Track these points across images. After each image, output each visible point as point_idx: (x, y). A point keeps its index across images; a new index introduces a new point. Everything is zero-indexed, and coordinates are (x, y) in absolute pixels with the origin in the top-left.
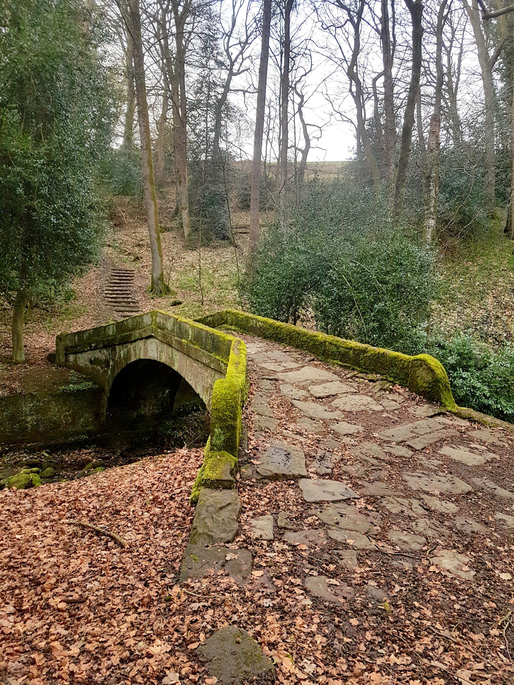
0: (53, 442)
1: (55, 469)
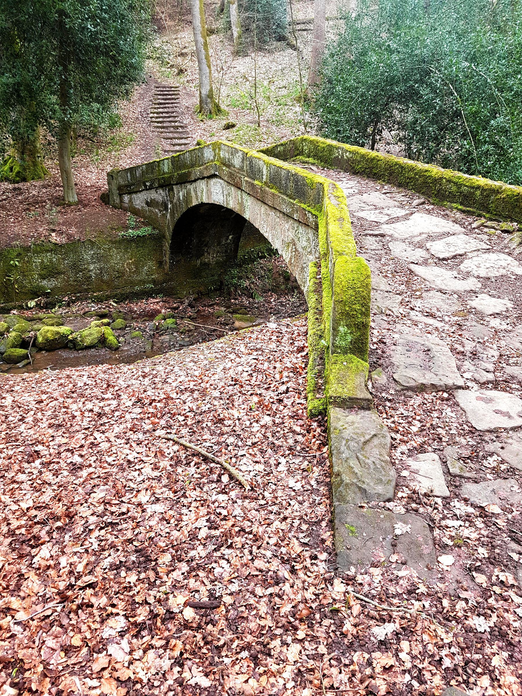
0: (119, 291)
1: (125, 319)
